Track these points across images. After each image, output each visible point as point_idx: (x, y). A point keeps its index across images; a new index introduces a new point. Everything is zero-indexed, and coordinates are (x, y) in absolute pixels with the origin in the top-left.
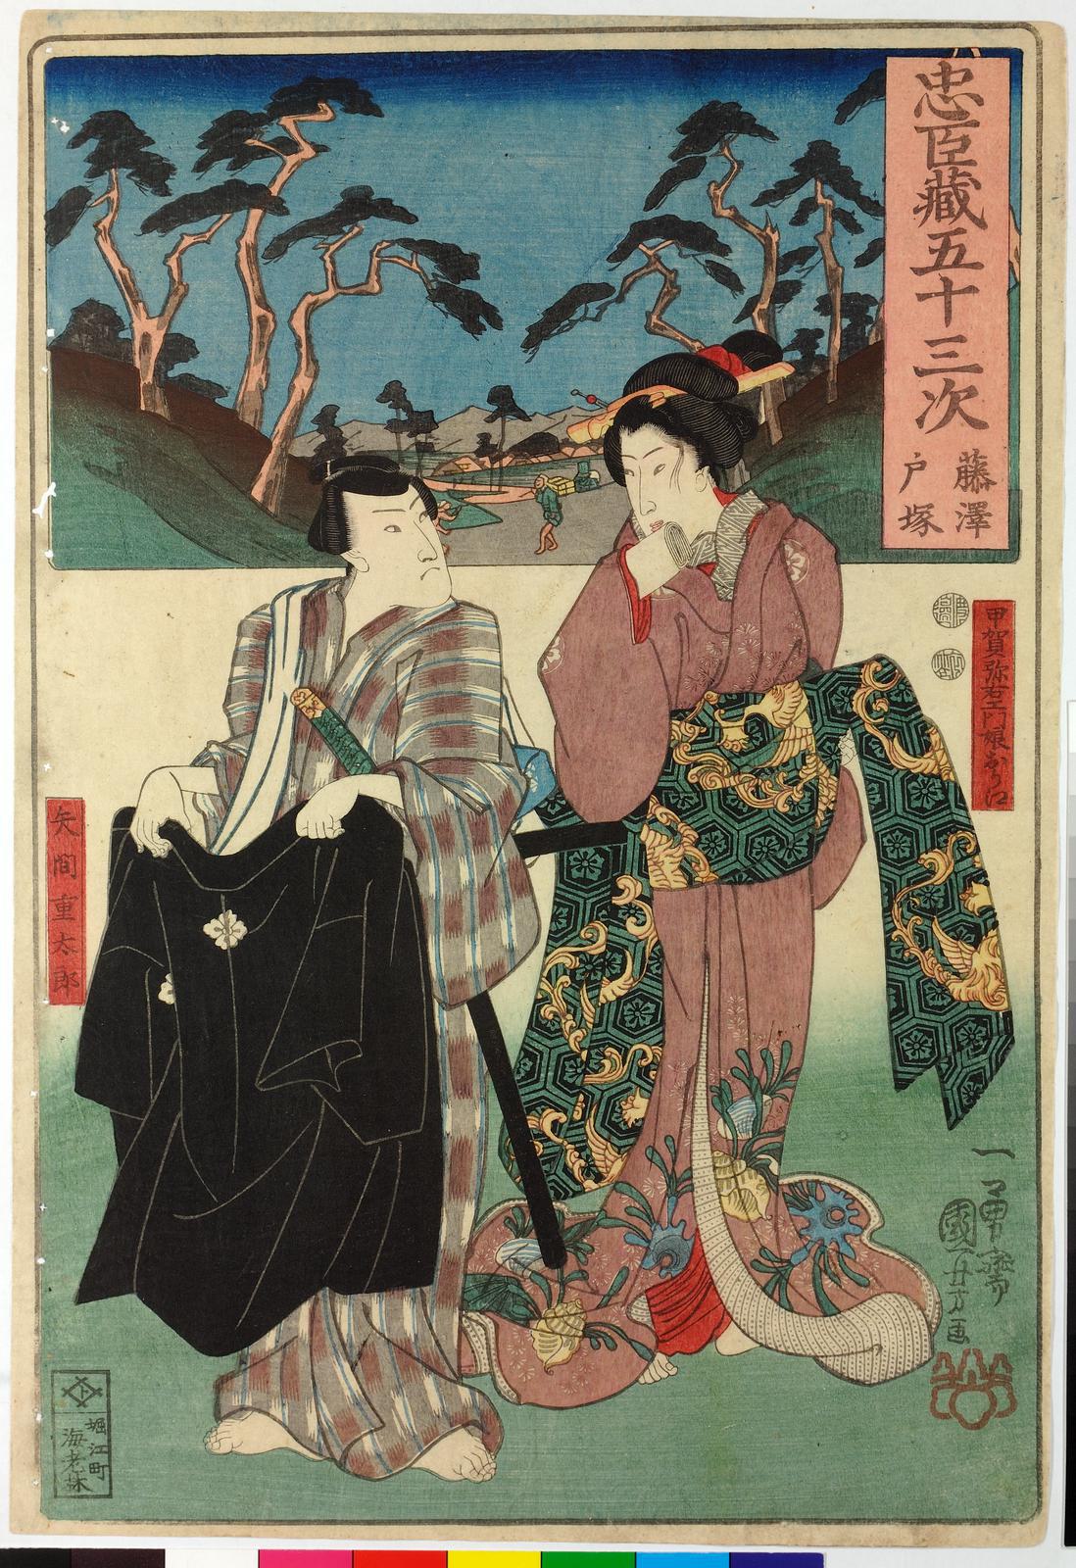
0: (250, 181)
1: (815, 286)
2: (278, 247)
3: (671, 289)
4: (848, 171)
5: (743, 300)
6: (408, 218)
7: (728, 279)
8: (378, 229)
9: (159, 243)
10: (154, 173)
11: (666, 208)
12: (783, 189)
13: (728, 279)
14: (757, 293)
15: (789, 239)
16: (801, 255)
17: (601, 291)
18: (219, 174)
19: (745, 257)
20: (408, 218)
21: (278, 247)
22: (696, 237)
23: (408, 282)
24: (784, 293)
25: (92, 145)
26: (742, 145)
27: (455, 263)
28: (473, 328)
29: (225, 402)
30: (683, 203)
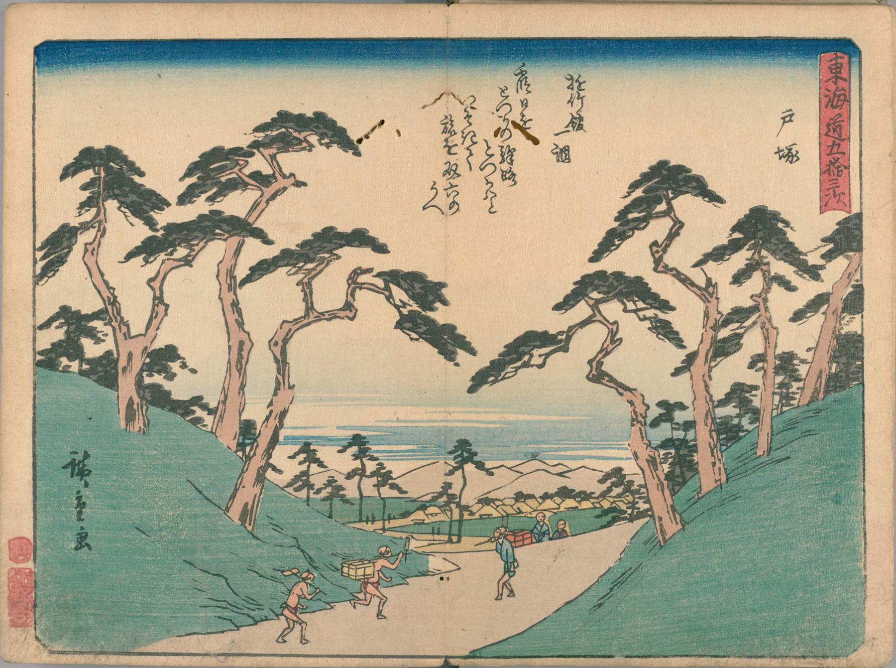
0: (228, 212)
1: (753, 343)
2: (261, 269)
3: (614, 339)
4: (470, 343)
5: (682, 354)
6: (381, 249)
7: (665, 330)
8: (354, 256)
9: (140, 271)
10: (144, 203)
11: (610, 264)
12: (718, 254)
13: (665, 330)
14: (696, 349)
15: (732, 297)
16: (740, 314)
17: (543, 339)
18: (201, 206)
19: (688, 316)
20: (381, 249)
21: (261, 269)
22: (632, 289)
23: (378, 312)
24: (723, 349)
25: (87, 175)
26: (686, 205)
27: (426, 291)
28: (450, 356)
29: (707, 199)
30: (633, 258)
